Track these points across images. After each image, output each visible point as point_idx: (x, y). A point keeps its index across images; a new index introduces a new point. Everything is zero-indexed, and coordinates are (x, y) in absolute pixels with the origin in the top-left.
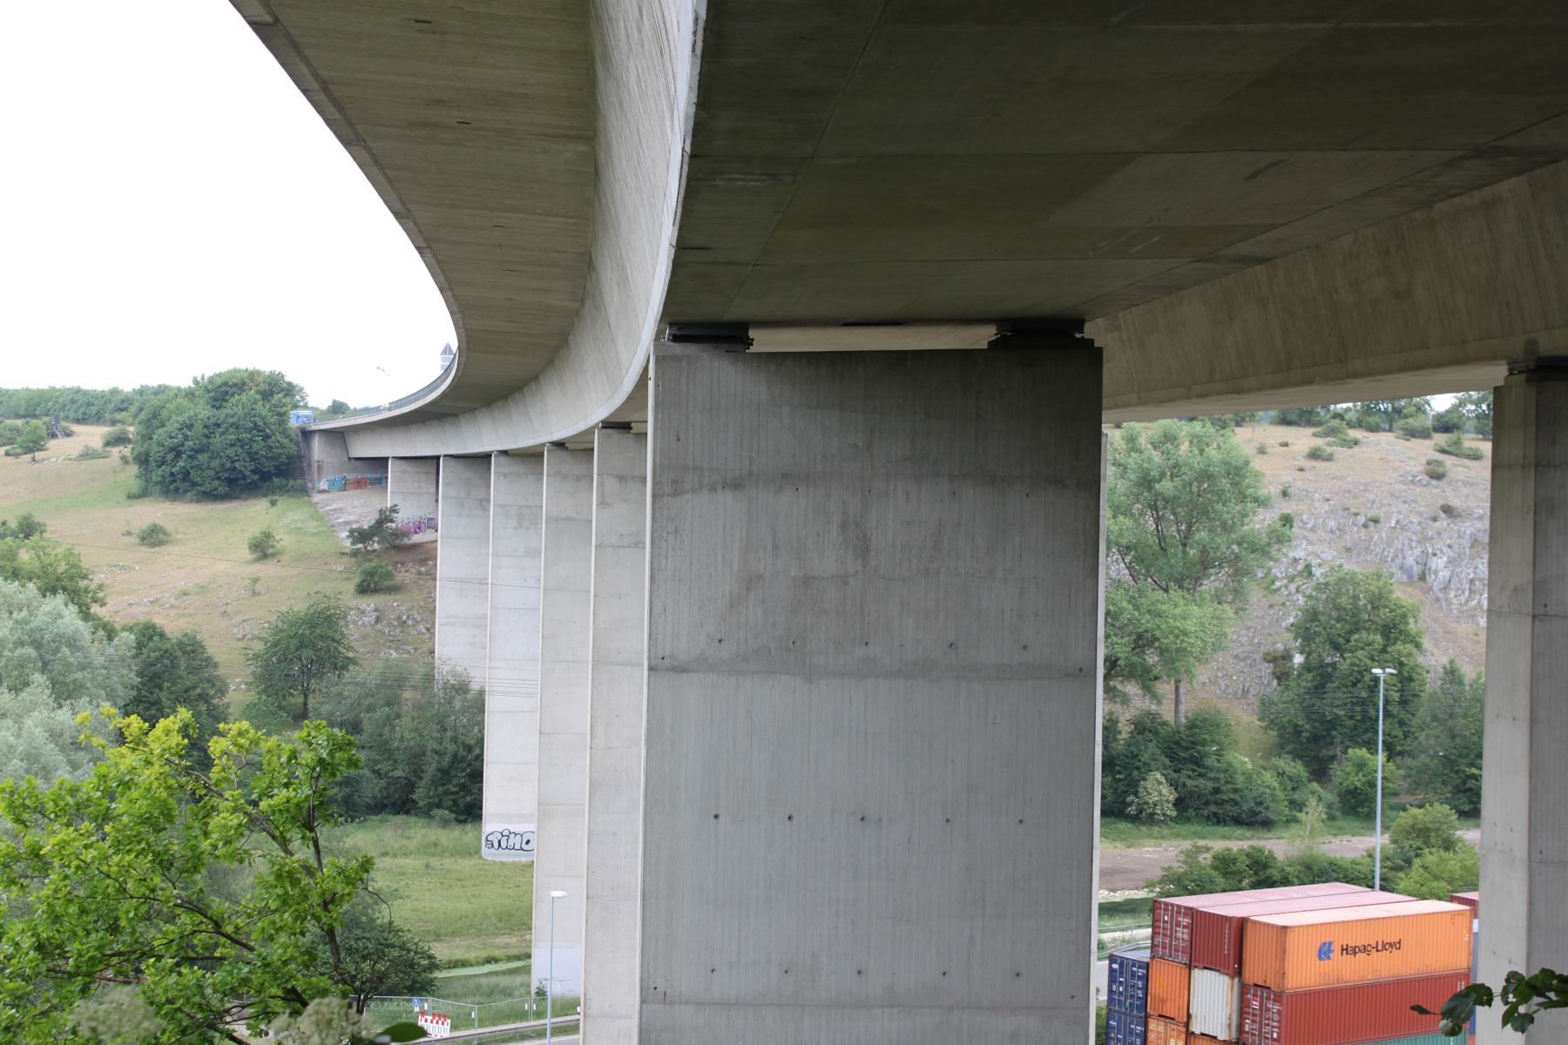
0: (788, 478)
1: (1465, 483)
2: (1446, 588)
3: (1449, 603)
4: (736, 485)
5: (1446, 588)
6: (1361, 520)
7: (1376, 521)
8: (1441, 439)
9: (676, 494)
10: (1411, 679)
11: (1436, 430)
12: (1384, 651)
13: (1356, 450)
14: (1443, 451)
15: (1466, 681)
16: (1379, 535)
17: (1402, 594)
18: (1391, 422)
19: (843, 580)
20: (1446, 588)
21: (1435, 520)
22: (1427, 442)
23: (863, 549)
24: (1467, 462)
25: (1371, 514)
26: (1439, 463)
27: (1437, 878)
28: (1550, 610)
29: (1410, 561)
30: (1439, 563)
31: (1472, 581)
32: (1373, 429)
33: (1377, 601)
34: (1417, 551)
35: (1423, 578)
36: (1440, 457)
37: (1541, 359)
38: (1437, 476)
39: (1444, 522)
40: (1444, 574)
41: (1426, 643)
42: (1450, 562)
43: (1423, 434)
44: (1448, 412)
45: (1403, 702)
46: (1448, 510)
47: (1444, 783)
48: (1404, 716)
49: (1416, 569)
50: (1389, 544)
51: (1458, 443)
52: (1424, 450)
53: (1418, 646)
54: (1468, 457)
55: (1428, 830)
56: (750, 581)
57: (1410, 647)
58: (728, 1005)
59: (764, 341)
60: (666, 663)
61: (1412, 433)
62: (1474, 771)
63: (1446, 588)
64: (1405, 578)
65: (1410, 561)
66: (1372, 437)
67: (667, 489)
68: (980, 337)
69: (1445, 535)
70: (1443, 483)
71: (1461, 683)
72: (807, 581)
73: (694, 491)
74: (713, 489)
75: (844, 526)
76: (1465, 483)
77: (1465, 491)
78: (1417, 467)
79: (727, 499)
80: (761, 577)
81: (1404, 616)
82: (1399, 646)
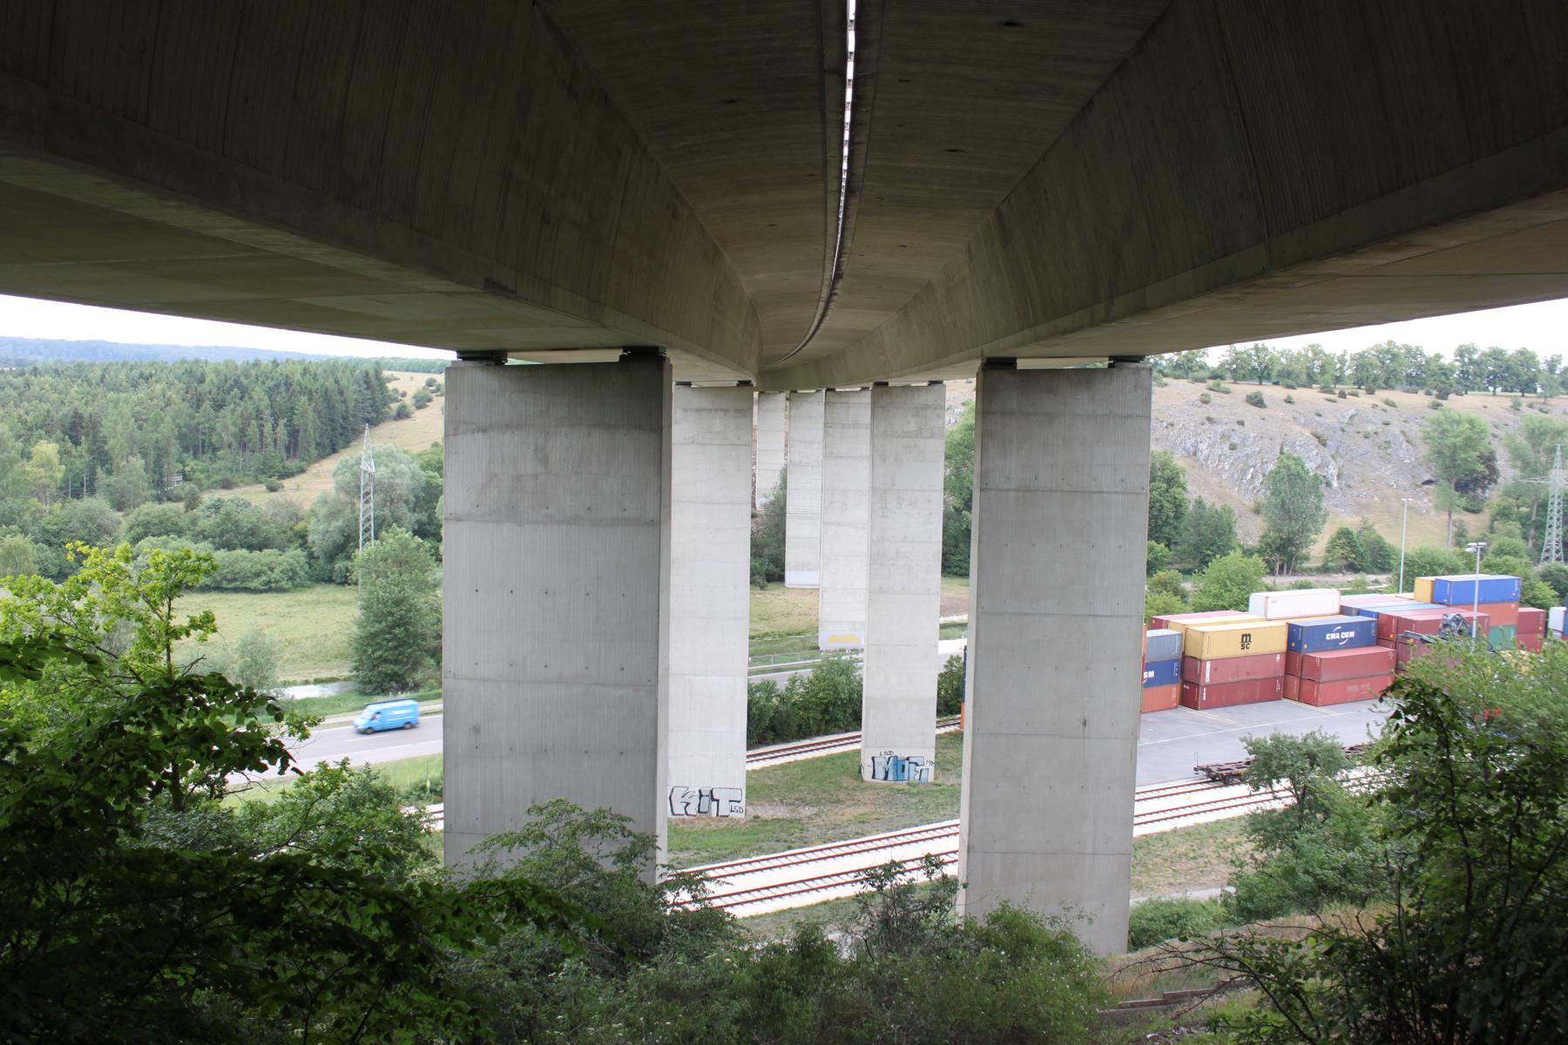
0: (508, 427)
1: (1220, 406)
2: (1206, 460)
3: (1208, 467)
4: (484, 430)
5: (1206, 459)
6: (1165, 424)
7: (1172, 425)
8: (1211, 383)
9: (455, 435)
10: (1180, 506)
11: (1210, 378)
12: (1167, 491)
13: (1166, 388)
14: (1211, 389)
15: (1208, 507)
16: (1173, 432)
17: (1179, 462)
18: (1187, 374)
19: (535, 477)
20: (1206, 460)
21: (1203, 424)
22: (1204, 385)
23: (545, 461)
24: (1222, 394)
25: (1170, 421)
26: (1206, 395)
27: (1152, 608)
28: (989, 487)
29: (1189, 445)
30: (1203, 446)
31: (1220, 456)
32: (1177, 378)
33: (1165, 466)
34: (1193, 440)
35: (1195, 454)
36: (1208, 392)
37: (988, 359)
38: (1205, 402)
39: (1207, 425)
40: (1206, 452)
41: (1189, 487)
42: (1209, 445)
43: (1202, 380)
44: (1218, 369)
45: (1176, 518)
46: (1209, 419)
47: (1194, 558)
48: (1176, 524)
49: (1192, 450)
50: (1178, 436)
51: (1218, 385)
52: (1201, 388)
53: (1184, 489)
54: (1223, 392)
55: (1166, 583)
56: (492, 477)
57: (1180, 489)
58: (484, 680)
59: (511, 361)
60: (452, 516)
61: (1197, 380)
62: (965, 565)
63: (1206, 459)
64: (1186, 454)
65: (1189, 445)
66: (1175, 381)
67: (452, 432)
68: (614, 356)
69: (1208, 433)
70: (1208, 406)
71: (1204, 508)
72: (518, 477)
73: (464, 433)
74: (473, 432)
75: (536, 450)
76: (1220, 406)
77: (1219, 409)
78: (1196, 397)
79: (479, 437)
80: (496, 475)
81: (1178, 473)
82: (1174, 489)
